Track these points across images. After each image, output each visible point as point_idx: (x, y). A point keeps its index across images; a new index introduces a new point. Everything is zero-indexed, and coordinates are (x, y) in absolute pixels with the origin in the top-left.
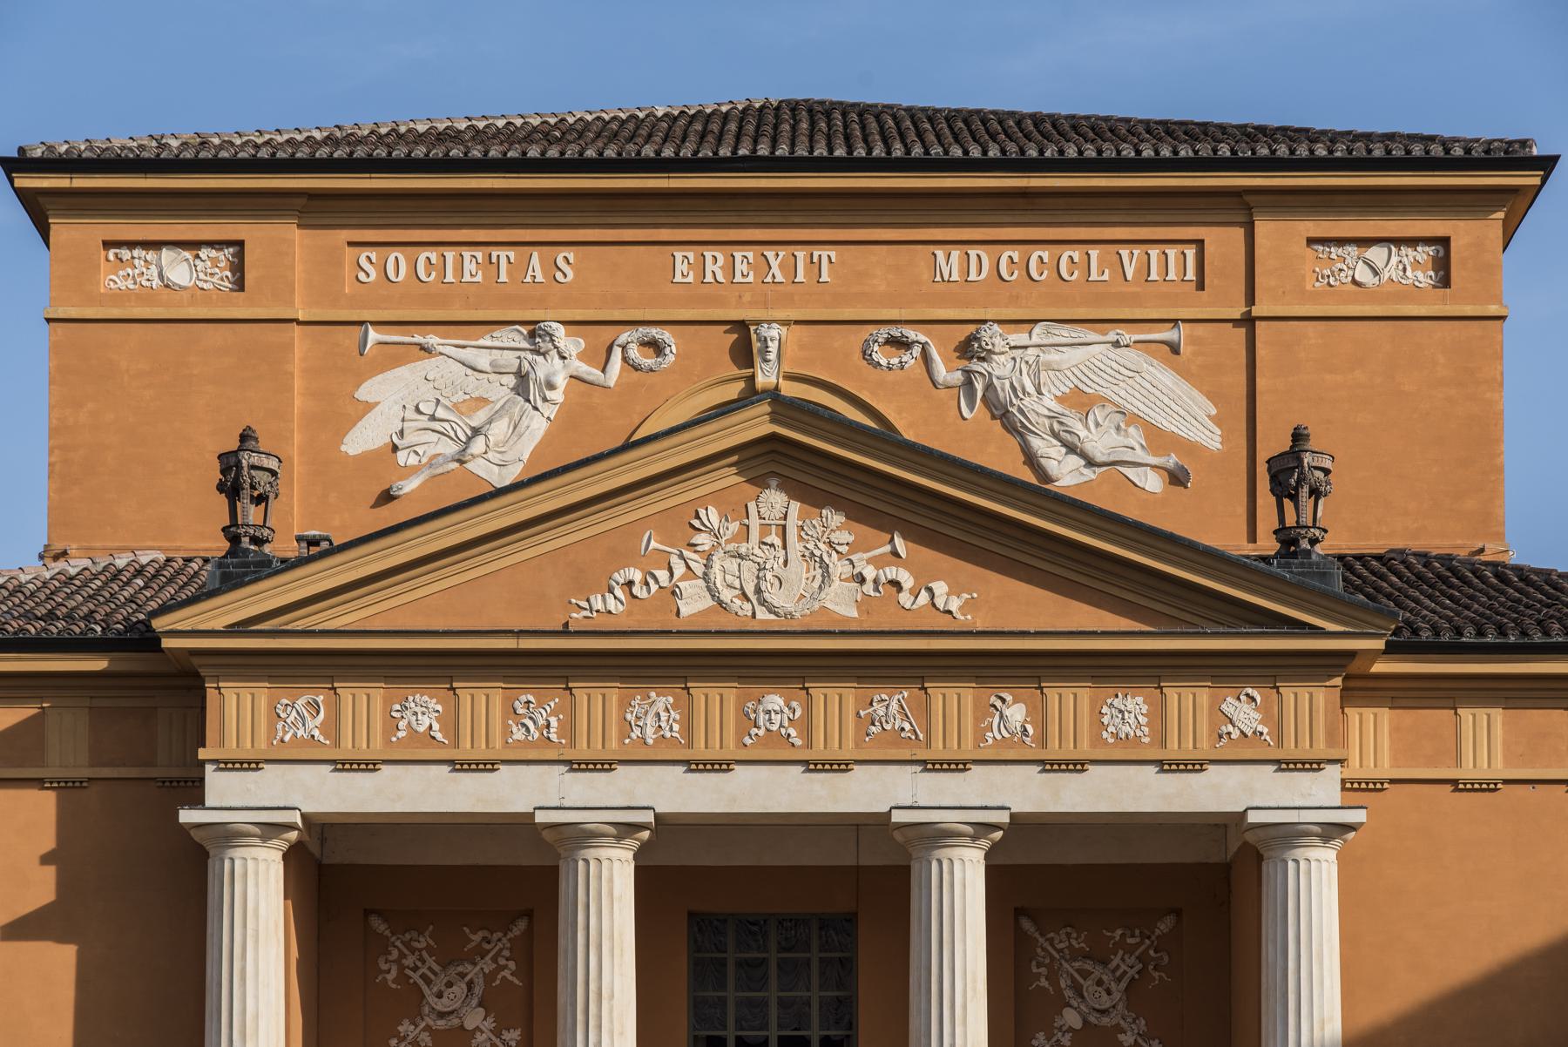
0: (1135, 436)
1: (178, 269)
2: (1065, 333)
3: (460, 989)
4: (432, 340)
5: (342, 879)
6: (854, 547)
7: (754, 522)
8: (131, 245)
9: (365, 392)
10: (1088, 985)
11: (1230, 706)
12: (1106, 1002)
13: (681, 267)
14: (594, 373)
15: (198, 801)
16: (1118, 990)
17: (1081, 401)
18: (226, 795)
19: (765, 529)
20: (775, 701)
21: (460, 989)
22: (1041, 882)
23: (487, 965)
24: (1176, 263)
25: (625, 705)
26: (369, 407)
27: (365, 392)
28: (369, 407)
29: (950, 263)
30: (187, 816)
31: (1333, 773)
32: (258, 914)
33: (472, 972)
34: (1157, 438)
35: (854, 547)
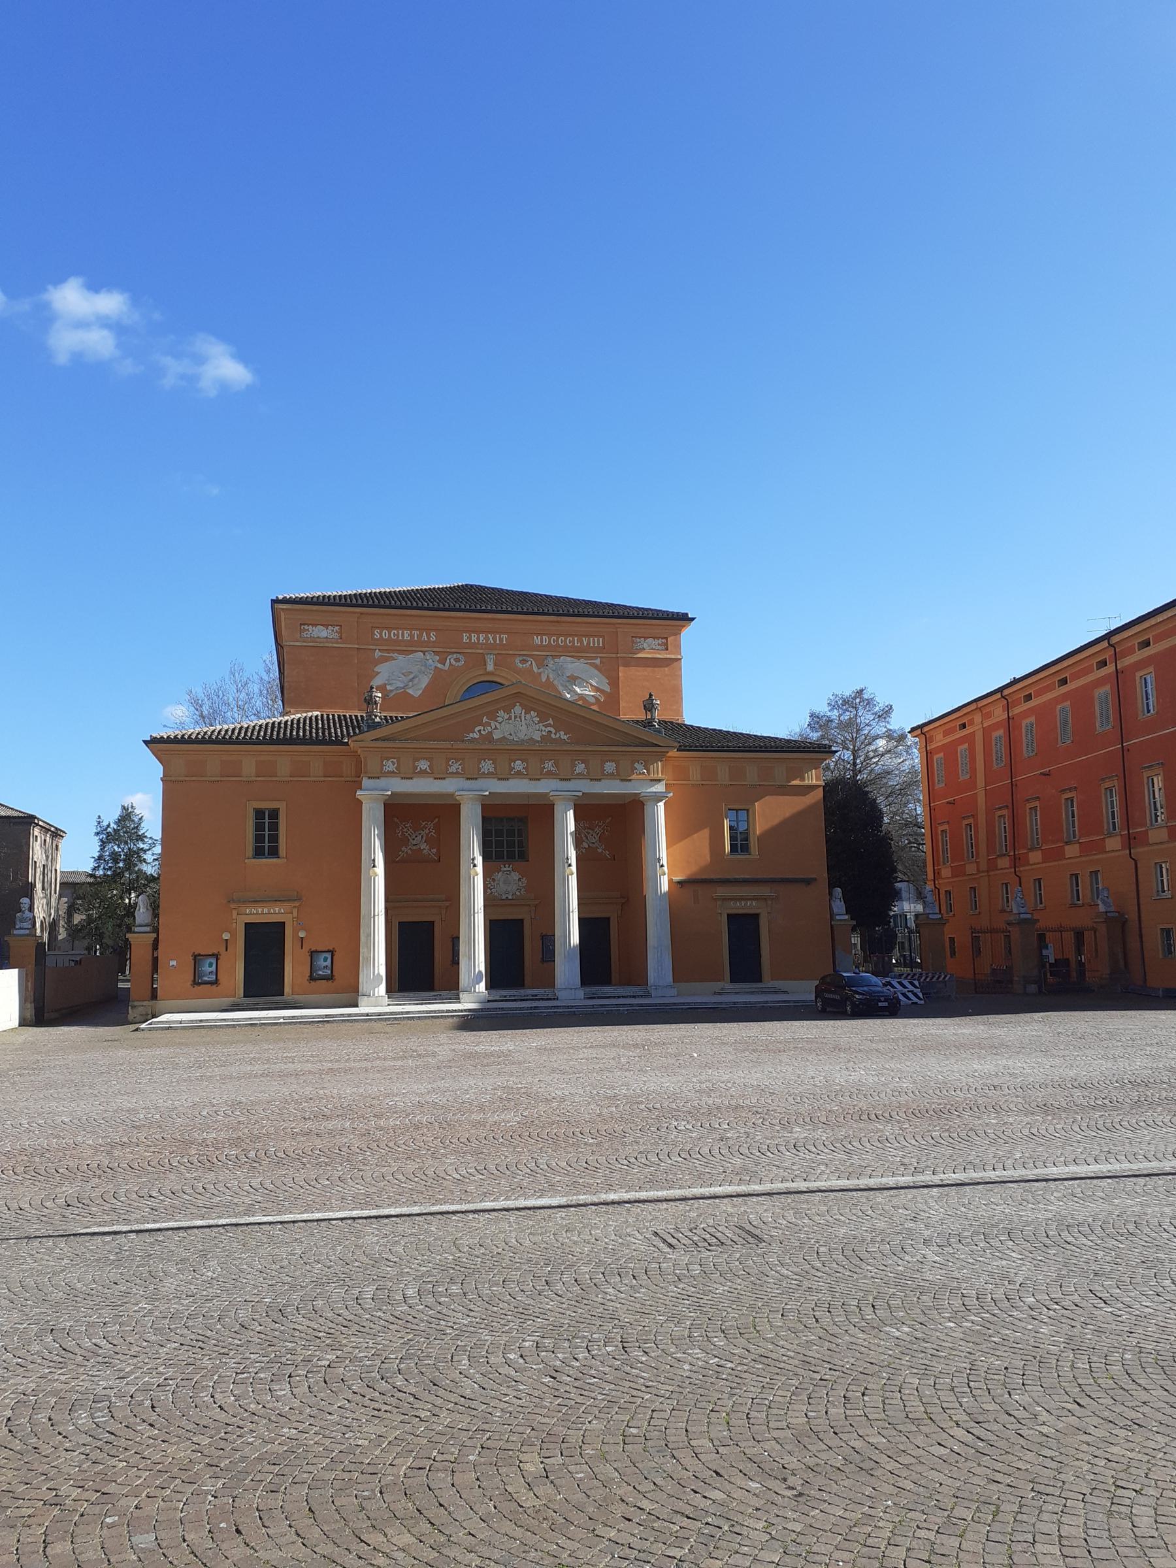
1: (322, 632)
2: (569, 659)
5: (398, 813)
9: (376, 669)
14: (439, 665)
24: (598, 642)
26: (378, 673)
27: (376, 669)
28: (378, 673)
29: (537, 640)
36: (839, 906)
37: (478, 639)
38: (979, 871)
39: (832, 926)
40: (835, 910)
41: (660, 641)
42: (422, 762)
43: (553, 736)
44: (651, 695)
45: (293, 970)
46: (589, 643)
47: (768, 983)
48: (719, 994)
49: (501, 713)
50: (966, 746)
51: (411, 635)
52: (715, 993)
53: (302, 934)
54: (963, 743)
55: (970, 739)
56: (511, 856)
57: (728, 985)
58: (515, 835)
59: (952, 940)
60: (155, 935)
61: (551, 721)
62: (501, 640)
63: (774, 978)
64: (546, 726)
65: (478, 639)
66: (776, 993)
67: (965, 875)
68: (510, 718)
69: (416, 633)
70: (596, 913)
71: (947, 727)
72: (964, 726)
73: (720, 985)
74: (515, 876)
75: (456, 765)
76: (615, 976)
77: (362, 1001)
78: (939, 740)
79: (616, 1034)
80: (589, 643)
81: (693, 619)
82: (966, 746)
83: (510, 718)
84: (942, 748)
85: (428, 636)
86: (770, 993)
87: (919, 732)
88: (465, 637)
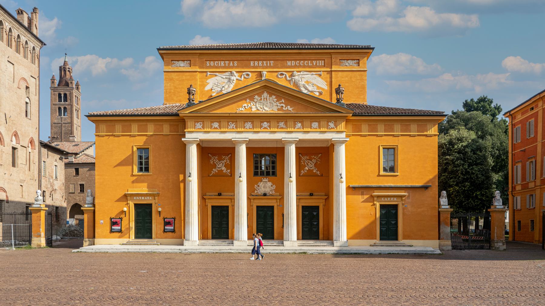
0: (315, 88)
3: (221, 164)
4: (217, 74)
5: (207, 151)
6: (277, 101)
7: (263, 98)
8: (344, 60)
9: (207, 81)
10: (309, 164)
11: (330, 124)
12: (311, 166)
13: (252, 64)
15: (184, 137)
16: (313, 164)
17: (308, 82)
18: (189, 137)
19: (264, 99)
20: (265, 123)
21: (221, 164)
22: (304, 151)
23: (225, 161)
25: (244, 124)
26: (208, 83)
27: (207, 81)
30: (183, 139)
31: (345, 133)
32: (193, 153)
33: (223, 162)
34: (318, 87)
35: (277, 101)
36: (444, 201)
37: (258, 64)
38: (535, 186)
39: (439, 212)
40: (442, 203)
41: (355, 61)
42: (215, 123)
43: (284, 109)
44: (339, 85)
45: (157, 226)
46: (316, 64)
47: (401, 241)
48: (373, 246)
49: (256, 97)
50: (533, 119)
51: (225, 63)
52: (371, 246)
53: (160, 209)
54: (532, 118)
55: (536, 115)
56: (268, 174)
57: (377, 241)
58: (266, 162)
59: (519, 222)
60: (92, 208)
61: (283, 101)
62: (270, 64)
63: (404, 238)
64: (280, 103)
65: (258, 64)
66: (404, 246)
67: (528, 188)
68: (261, 99)
69: (227, 62)
70: (310, 202)
71: (523, 111)
72: (532, 109)
73: (373, 242)
74: (270, 184)
75: (233, 125)
76: (321, 236)
77: (186, 243)
78: (519, 118)
79: (453, 263)
80: (316, 64)
81: (373, 49)
82: (533, 119)
83: (261, 99)
84: (521, 122)
85: (233, 64)
86: (400, 246)
87: (508, 114)
88: (236, 65)
